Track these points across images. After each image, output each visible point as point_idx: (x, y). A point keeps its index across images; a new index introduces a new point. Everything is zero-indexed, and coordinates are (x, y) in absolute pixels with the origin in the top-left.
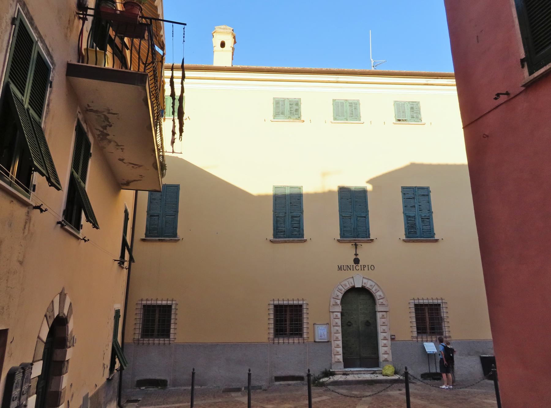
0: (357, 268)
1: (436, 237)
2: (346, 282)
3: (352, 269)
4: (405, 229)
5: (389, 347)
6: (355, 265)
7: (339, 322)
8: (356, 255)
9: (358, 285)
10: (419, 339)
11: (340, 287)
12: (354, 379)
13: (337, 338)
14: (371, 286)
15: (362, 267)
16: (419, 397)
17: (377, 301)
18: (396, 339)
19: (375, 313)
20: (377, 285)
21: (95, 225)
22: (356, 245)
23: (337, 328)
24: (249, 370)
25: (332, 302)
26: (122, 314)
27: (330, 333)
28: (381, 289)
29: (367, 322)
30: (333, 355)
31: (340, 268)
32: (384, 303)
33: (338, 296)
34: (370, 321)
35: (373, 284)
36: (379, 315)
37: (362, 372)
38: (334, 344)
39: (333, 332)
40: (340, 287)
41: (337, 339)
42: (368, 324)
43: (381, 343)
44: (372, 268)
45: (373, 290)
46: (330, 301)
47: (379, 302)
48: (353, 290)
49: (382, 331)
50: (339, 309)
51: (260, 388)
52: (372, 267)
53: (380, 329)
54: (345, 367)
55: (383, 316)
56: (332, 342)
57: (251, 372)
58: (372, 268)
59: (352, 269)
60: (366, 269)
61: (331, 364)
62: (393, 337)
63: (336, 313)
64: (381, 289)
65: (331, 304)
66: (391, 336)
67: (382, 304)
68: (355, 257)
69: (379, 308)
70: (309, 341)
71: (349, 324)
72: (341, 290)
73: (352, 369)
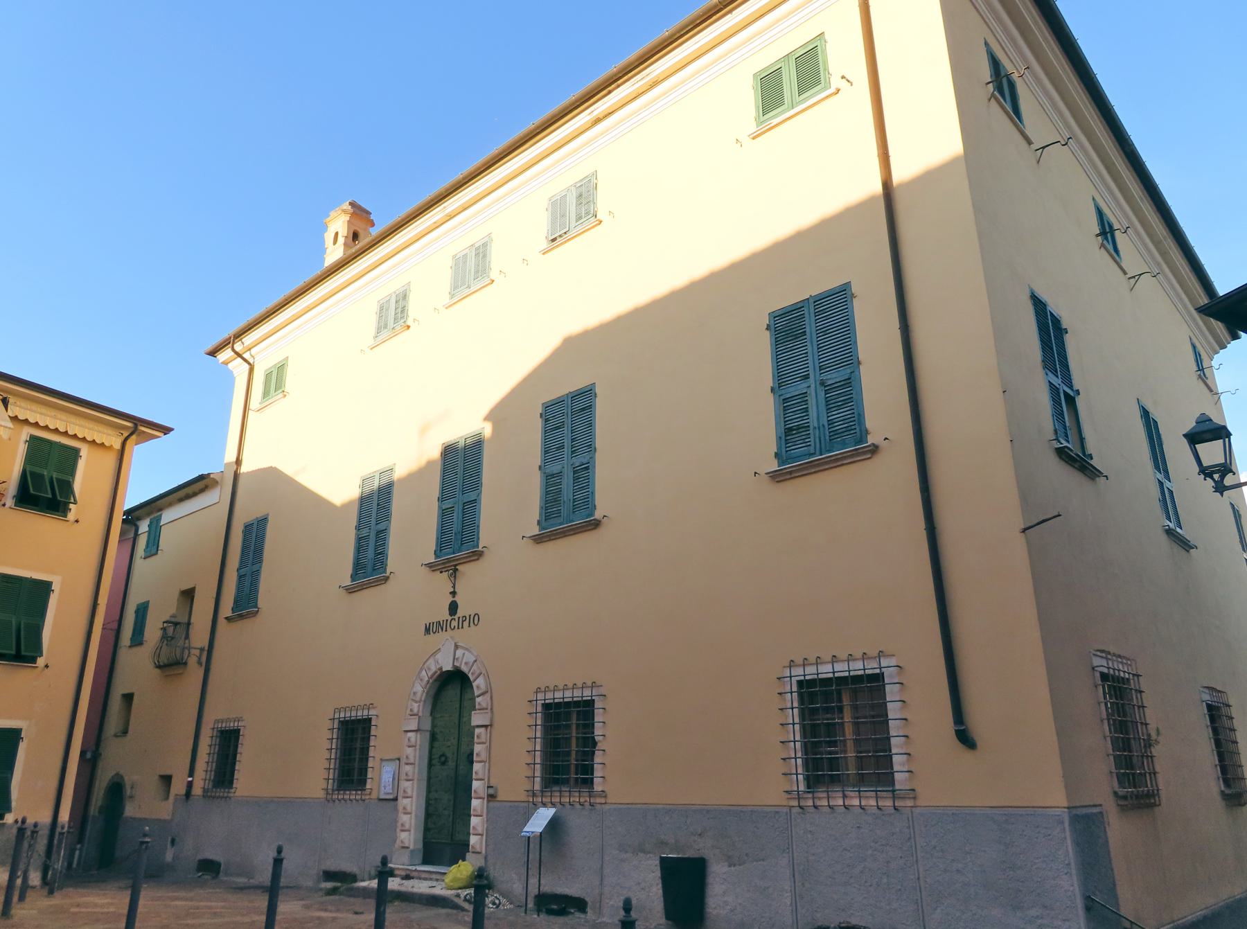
1: (598, 515)
4: (541, 508)
8: (454, 593)
24: (280, 851)
27: (397, 779)
37: (434, 876)
38: (403, 802)
51: (297, 888)
57: (283, 855)
60: (466, 624)
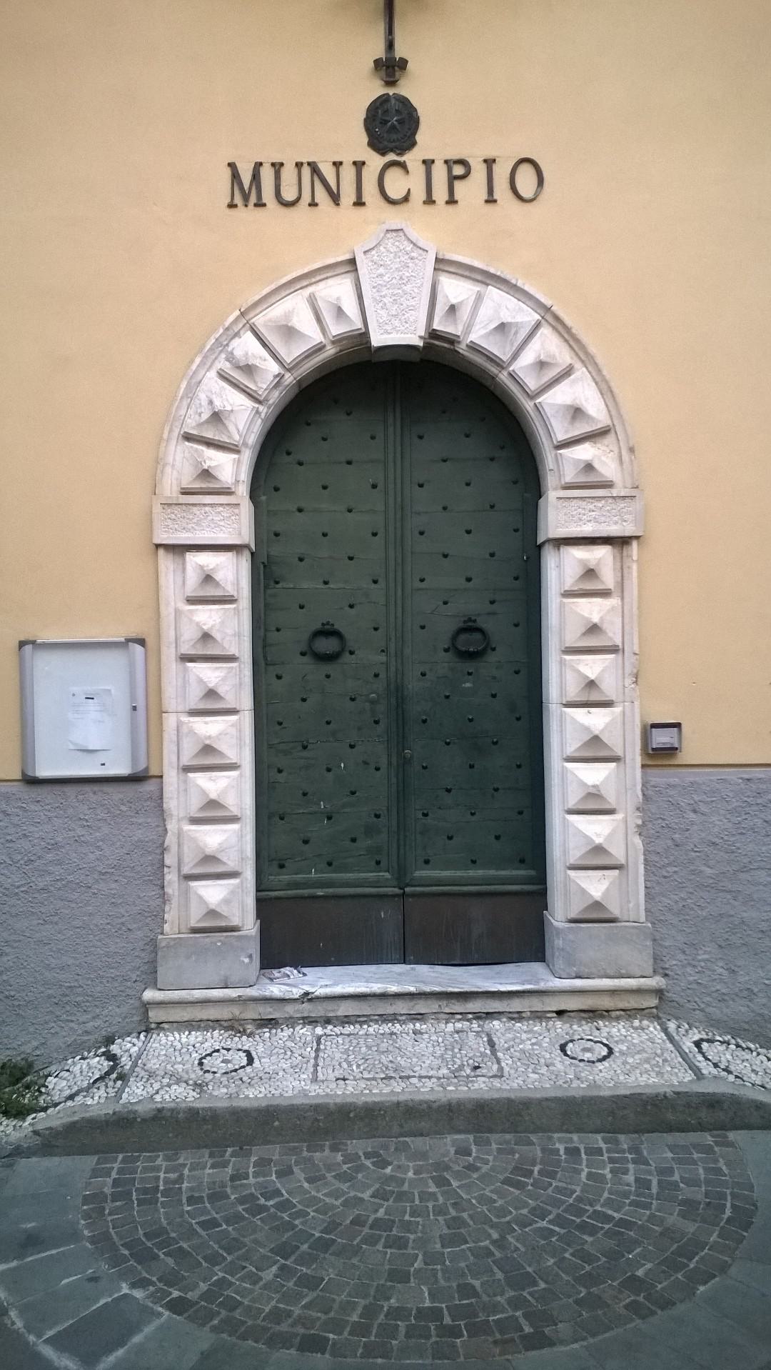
0: (396, 184)
2: (295, 309)
3: (348, 195)
6: (376, 162)
7: (232, 626)
8: (391, 68)
9: (397, 329)
11: (246, 346)
14: (502, 327)
15: (439, 173)
17: (549, 458)
18: (685, 757)
20: (550, 317)
21: (232, 166)
23: (210, 674)
25: (180, 464)
27: (147, 714)
28: (587, 359)
30: (171, 877)
31: (246, 189)
33: (217, 417)
35: (529, 316)
36: (560, 570)
38: (182, 793)
39: (171, 698)
40: (246, 346)
41: (209, 759)
43: (569, 778)
46: (158, 462)
47: (561, 466)
49: (573, 692)
50: (234, 522)
53: (562, 675)
55: (590, 573)
56: (171, 778)
59: (348, 195)
60: (470, 191)
61: (153, 945)
62: (662, 738)
63: (579, 553)
64: (587, 359)
65: (170, 487)
66: (650, 728)
68: (376, 89)
69: (560, 515)
72: (249, 369)
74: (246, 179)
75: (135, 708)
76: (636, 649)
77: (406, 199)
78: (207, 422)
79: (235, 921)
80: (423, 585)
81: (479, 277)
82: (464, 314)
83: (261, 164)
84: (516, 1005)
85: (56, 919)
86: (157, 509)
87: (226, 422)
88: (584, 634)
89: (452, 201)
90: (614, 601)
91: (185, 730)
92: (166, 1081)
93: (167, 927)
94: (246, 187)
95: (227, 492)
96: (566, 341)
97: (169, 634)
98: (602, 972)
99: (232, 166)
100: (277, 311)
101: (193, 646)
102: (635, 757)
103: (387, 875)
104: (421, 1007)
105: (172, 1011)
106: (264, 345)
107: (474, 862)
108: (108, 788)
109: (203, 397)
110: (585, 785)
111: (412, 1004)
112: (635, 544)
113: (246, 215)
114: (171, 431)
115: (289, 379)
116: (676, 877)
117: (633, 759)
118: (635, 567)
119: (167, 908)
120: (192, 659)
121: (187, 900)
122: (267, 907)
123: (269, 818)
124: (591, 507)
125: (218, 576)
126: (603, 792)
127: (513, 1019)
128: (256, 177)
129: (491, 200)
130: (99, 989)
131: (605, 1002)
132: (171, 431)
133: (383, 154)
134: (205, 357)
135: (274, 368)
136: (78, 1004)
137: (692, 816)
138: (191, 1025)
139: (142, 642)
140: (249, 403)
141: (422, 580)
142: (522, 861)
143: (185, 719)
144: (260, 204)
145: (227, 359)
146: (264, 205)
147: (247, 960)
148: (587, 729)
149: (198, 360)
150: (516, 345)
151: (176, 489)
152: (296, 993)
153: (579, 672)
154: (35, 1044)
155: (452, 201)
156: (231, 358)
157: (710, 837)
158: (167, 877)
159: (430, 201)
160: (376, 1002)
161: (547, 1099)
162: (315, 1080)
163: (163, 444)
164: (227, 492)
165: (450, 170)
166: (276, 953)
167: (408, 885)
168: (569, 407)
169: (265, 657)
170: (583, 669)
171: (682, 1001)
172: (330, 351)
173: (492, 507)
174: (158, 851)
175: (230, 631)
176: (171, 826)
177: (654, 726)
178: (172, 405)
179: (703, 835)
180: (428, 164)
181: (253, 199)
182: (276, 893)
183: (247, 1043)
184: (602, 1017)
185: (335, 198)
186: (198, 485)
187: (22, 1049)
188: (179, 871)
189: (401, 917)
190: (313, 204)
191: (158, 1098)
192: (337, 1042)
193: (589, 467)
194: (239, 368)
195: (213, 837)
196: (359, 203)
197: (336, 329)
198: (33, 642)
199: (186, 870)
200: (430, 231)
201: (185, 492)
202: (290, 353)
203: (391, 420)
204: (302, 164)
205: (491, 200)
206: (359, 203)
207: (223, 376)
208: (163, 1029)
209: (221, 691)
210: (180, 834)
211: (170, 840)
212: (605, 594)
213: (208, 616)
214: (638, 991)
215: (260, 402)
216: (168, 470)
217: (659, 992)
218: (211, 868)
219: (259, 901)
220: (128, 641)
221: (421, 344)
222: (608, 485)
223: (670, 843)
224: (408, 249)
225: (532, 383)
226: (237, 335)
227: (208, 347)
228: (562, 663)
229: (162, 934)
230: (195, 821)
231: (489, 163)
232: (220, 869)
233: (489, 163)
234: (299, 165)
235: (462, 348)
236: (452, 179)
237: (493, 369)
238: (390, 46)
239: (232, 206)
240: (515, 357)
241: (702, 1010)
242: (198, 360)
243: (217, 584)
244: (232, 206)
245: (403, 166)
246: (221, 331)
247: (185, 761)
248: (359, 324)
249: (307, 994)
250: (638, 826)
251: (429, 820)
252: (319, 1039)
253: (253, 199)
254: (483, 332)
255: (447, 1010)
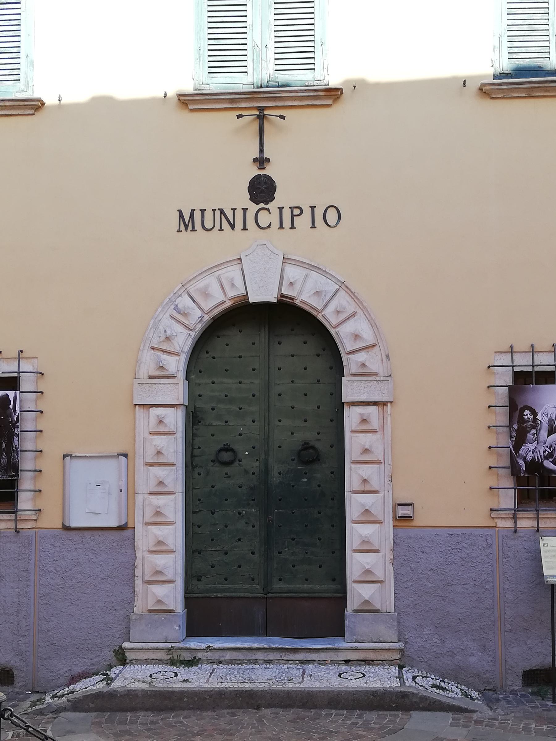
2: (211, 282)
3: (239, 224)
5: (387, 553)
6: (253, 208)
7: (174, 448)
8: (262, 161)
9: (263, 293)
10: (521, 523)
11: (185, 302)
12: (215, 684)
13: (158, 513)
16: (38, 703)
18: (416, 523)
19: (339, 408)
21: (180, 211)
22: (261, 118)
25: (148, 364)
26: (239, 113)
27: (129, 492)
28: (364, 309)
29: (306, 446)
30: (138, 582)
31: (186, 222)
32: (373, 366)
34: (318, 445)
36: (352, 417)
37: (260, 656)
38: (144, 537)
40: (185, 302)
41: (158, 519)
42: (308, 455)
43: (356, 533)
44: (332, 216)
45: (329, 317)
46: (138, 362)
47: (351, 363)
48: (241, 316)
50: (177, 392)
52: (329, 216)
53: (353, 476)
54: (194, 629)
55: (364, 421)
56: (139, 530)
58: (332, 216)
59: (239, 224)
60: (303, 221)
61: (128, 621)
62: (403, 511)
65: (143, 373)
67: (366, 374)
68: (255, 172)
69: (351, 390)
70: (40, 524)
71: (226, 456)
72: (185, 315)
73: (218, 643)
74: (187, 217)
75: (121, 491)
76: (390, 463)
77: (269, 226)
78: (163, 341)
79: (171, 607)
80: (280, 424)
81: (307, 266)
82: (298, 286)
83: (195, 210)
84: (323, 656)
85: (78, 603)
86: (136, 385)
87: (173, 341)
88: (362, 454)
89: (293, 227)
90: (379, 436)
91: (147, 503)
92: (133, 681)
93: (135, 609)
94: (187, 222)
95: (173, 377)
96: (352, 298)
97: (139, 451)
98: (370, 639)
99: (180, 211)
100: (201, 284)
101: (152, 458)
102: (389, 522)
103: (258, 587)
104: (271, 656)
105: (138, 654)
106: (194, 301)
107: (307, 580)
108: (106, 533)
109: (161, 328)
110: (361, 536)
111: (266, 654)
112: (389, 405)
113: (187, 235)
114: (144, 346)
115: (207, 318)
116: (412, 588)
117: (389, 523)
118: (389, 418)
119: (136, 599)
120: (151, 465)
121: (147, 595)
122: (190, 600)
123: (193, 553)
124: (365, 386)
125: (166, 421)
126: (371, 540)
127: (321, 664)
128: (192, 216)
129: (313, 226)
130: (100, 641)
131: (371, 656)
132: (144, 346)
133: (258, 204)
134: (164, 308)
135: (199, 313)
136: (88, 649)
137: (421, 554)
138: (147, 662)
139: (126, 455)
140: (186, 332)
141: (280, 421)
142: (334, 580)
143: (147, 496)
144: (193, 230)
145: (174, 309)
146: (196, 231)
147: (177, 628)
148: (363, 505)
149: (160, 309)
150: (325, 301)
151: (146, 376)
152: (203, 646)
153: (359, 474)
154: (66, 670)
155: (293, 227)
156: (176, 309)
157: (431, 566)
158: (136, 582)
159: (281, 227)
160: (246, 653)
161: (320, 691)
162: (207, 682)
163: (140, 352)
164: (173, 377)
165: (292, 212)
166: (194, 629)
167: (269, 593)
168: (353, 334)
169: (192, 463)
170: (360, 472)
171: (415, 657)
172: (228, 304)
173: (319, 381)
174: (132, 568)
175: (172, 450)
176: (139, 554)
177: (399, 505)
178: (145, 332)
179: (427, 565)
180: (281, 209)
181: (190, 227)
182: (197, 595)
183: (175, 669)
184: (369, 664)
185: (233, 227)
186: (157, 373)
187: (59, 672)
188: (143, 579)
189: (265, 610)
190: (221, 230)
191: (128, 686)
192: (222, 670)
193: (363, 365)
194: (179, 312)
195: (161, 561)
196: (245, 229)
197: (232, 293)
198: (71, 455)
199: (147, 578)
200: (282, 241)
201: (150, 377)
202: (208, 305)
203: (263, 335)
204: (215, 210)
205: (313, 226)
206: (245, 229)
207: (172, 317)
208: (133, 663)
209: (166, 482)
210: (143, 558)
211: (138, 563)
212: (374, 431)
213: (160, 441)
214: (389, 650)
215: (191, 330)
216: (142, 365)
217: (401, 651)
218: (159, 578)
219: (186, 599)
220: (119, 455)
221: (276, 301)
222: (376, 374)
223: (409, 569)
224: (269, 254)
225: (334, 322)
226: (180, 296)
227: (165, 303)
228: (351, 469)
229: (133, 612)
230: (152, 552)
231: (313, 208)
232: (164, 578)
233: (313, 208)
234: (214, 210)
235: (297, 302)
236: (293, 216)
237: (315, 313)
238: (262, 151)
239: (179, 231)
240: (325, 306)
241: (426, 662)
242: (160, 309)
243: (166, 425)
244: (179, 231)
245: (268, 210)
246: (172, 295)
247: (147, 519)
248: (243, 291)
249: (209, 647)
250: (391, 559)
251: (282, 556)
252: (213, 670)
253: (190, 227)
254: (308, 295)
255: (285, 658)
